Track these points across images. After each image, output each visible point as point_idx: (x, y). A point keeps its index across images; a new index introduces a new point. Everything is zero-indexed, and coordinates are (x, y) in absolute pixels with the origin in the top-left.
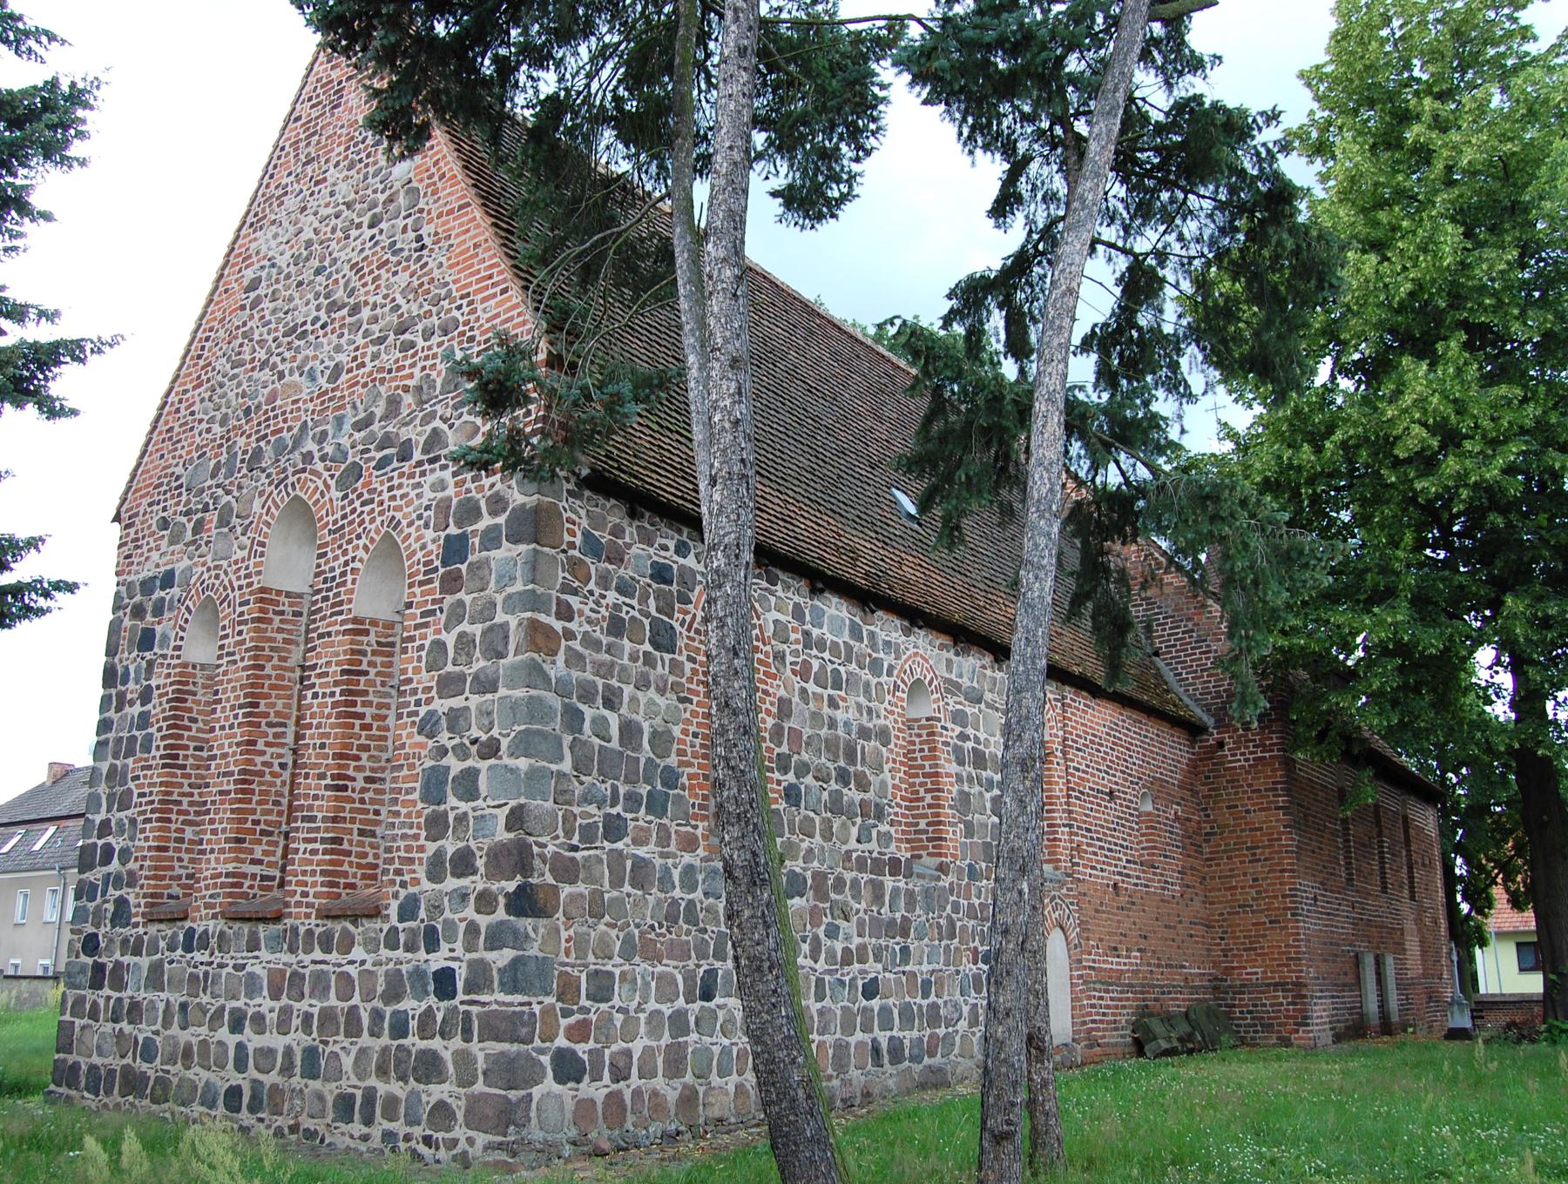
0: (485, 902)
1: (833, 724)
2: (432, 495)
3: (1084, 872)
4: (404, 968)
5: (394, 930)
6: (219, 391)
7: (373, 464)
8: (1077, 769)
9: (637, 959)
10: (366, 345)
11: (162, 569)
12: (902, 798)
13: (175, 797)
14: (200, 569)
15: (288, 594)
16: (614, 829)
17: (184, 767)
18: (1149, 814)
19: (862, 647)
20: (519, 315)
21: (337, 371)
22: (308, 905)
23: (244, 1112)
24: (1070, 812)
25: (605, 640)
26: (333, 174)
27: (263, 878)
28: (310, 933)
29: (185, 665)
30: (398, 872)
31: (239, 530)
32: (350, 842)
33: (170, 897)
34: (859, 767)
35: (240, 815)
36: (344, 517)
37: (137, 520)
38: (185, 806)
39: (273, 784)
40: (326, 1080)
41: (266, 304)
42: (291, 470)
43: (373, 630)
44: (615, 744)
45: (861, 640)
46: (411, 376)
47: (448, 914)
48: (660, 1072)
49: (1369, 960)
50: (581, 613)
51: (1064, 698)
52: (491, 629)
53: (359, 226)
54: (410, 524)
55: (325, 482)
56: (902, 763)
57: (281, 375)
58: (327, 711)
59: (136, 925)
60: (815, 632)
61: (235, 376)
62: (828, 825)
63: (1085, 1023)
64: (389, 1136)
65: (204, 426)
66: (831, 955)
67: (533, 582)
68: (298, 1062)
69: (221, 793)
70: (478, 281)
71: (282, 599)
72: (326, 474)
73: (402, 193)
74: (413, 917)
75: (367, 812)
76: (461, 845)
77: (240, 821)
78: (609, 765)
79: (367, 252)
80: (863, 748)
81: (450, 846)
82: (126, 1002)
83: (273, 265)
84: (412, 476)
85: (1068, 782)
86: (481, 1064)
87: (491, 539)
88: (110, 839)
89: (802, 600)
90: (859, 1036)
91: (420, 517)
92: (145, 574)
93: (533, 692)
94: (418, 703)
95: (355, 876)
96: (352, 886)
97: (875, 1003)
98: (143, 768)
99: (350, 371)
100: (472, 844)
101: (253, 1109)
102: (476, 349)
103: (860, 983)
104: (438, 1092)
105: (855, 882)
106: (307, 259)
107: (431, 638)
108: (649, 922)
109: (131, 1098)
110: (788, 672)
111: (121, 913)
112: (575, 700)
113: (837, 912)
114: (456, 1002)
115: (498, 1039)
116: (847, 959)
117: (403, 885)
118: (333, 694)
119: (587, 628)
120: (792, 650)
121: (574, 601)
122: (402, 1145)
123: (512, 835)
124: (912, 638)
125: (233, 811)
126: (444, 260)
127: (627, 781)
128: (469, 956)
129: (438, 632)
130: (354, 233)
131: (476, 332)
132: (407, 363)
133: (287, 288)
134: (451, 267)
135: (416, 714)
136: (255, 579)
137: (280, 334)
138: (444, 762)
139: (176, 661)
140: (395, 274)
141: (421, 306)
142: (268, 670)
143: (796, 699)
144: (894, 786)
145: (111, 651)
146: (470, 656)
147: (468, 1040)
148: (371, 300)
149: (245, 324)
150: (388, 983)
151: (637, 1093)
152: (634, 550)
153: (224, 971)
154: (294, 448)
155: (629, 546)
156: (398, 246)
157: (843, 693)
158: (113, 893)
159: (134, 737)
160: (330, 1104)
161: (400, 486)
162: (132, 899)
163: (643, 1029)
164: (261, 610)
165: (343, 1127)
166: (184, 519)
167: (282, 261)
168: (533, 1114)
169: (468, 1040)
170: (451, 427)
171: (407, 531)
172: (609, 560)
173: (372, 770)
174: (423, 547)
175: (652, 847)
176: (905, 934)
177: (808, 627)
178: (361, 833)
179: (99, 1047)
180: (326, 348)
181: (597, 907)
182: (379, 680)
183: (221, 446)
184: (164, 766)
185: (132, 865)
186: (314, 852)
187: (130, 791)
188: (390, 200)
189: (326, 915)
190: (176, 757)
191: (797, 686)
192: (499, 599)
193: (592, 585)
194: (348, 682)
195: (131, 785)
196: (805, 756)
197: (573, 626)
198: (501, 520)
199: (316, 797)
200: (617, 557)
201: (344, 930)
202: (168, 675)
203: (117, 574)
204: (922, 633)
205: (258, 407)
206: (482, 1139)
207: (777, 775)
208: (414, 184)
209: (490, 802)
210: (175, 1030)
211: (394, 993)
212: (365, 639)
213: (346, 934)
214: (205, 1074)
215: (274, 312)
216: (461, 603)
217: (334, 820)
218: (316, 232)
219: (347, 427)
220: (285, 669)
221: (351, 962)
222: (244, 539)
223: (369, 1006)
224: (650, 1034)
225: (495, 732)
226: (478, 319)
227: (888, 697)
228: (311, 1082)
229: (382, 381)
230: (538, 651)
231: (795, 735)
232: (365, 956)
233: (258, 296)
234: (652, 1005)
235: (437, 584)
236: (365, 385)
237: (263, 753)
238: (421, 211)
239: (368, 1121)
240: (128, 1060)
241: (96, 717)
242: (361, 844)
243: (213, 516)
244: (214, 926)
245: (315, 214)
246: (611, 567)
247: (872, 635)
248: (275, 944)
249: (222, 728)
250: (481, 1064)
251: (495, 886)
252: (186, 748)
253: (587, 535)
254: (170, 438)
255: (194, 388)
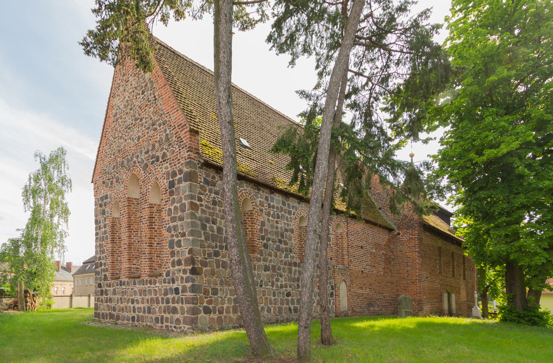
0: (185, 272)
1: (277, 228)
2: (165, 170)
3: (352, 267)
4: (168, 288)
5: (165, 279)
6: (112, 146)
7: (150, 163)
8: (351, 240)
9: (224, 285)
10: (145, 130)
11: (105, 194)
12: (297, 247)
13: (115, 250)
14: (113, 194)
15: (135, 199)
16: (217, 254)
17: (116, 243)
18: (374, 253)
19: (286, 207)
20: (182, 117)
21: (139, 138)
22: (146, 274)
23: (136, 322)
24: (348, 252)
25: (211, 207)
26: (131, 79)
27: (136, 268)
28: (147, 280)
29: (113, 218)
30: (165, 265)
31: (121, 183)
32: (154, 259)
33: (116, 273)
34: (285, 239)
35: (129, 254)
36: (145, 178)
37: (97, 182)
38: (117, 252)
39: (136, 246)
40: (153, 314)
41: (119, 120)
42: (131, 166)
43: (155, 207)
44: (216, 233)
45: (285, 205)
46: (157, 138)
47: (176, 275)
48: (231, 312)
49: (446, 295)
50: (204, 200)
51: (348, 221)
52: (181, 205)
53: (139, 94)
54: (161, 179)
55: (140, 169)
56: (297, 238)
57: (126, 140)
58: (146, 227)
59: (109, 280)
60: (272, 204)
61: (115, 141)
62: (276, 254)
63: (351, 306)
64: (167, 326)
65: (109, 156)
66: (277, 286)
67: (190, 192)
68: (146, 310)
69: (124, 248)
70: (171, 108)
71: (134, 200)
72: (139, 167)
73: (149, 83)
74: (169, 276)
75: (158, 251)
76: (178, 258)
77: (129, 255)
78: (214, 238)
79: (142, 102)
80: (286, 234)
81: (176, 259)
82: (109, 298)
83: (120, 108)
84: (160, 166)
85: (348, 243)
86: (186, 310)
87: (180, 181)
88: (101, 261)
89: (268, 195)
90: (285, 306)
91: (163, 176)
92: (101, 196)
93: (193, 220)
94: (166, 224)
95: (156, 267)
96: (156, 269)
97: (290, 298)
98: (107, 244)
99: (142, 138)
100: (181, 258)
101: (138, 321)
102: (172, 129)
103: (285, 293)
104: (177, 316)
105: (284, 268)
106: (128, 106)
107: (168, 208)
108: (227, 276)
109: (111, 320)
110: (264, 214)
111: (106, 278)
112: (204, 222)
113: (279, 275)
114: (179, 295)
115: (189, 304)
116: (282, 286)
117: (166, 268)
118: (147, 223)
119: (206, 203)
120: (265, 208)
121: (202, 197)
122: (170, 329)
123: (189, 255)
124: (301, 205)
125: (127, 253)
126: (161, 102)
127: (219, 242)
128: (182, 284)
129: (169, 206)
130: (138, 97)
131: (171, 124)
132: (156, 134)
133: (124, 115)
134: (163, 104)
135: (166, 227)
136: (126, 195)
137: (124, 129)
138: (174, 238)
139: (111, 217)
140: (150, 108)
141: (157, 117)
142: (132, 218)
143: (266, 221)
144: (295, 244)
145: (96, 216)
146: (177, 212)
147: (182, 304)
148: (145, 117)
149: (115, 126)
150: (164, 291)
151: (225, 317)
152: (219, 183)
153: (129, 290)
154: (131, 160)
155: (217, 181)
156: (150, 99)
157: (280, 220)
158: (103, 273)
159: (104, 236)
160: (154, 319)
161: (157, 168)
162: (107, 274)
163: (226, 302)
164: (128, 203)
165: (157, 325)
166: (108, 181)
167: (122, 107)
168: (199, 321)
169: (182, 304)
170: (168, 151)
171: (160, 180)
172: (211, 185)
173: (158, 241)
174: (164, 184)
175: (227, 258)
176: (298, 281)
177: (269, 202)
178: (157, 256)
179: (104, 309)
180: (136, 132)
181: (213, 273)
182: (158, 219)
183: (114, 161)
184: (111, 243)
185: (107, 267)
186: (146, 261)
187: (104, 249)
188: (146, 85)
189: (149, 276)
190: (114, 241)
191: (266, 218)
192: (183, 196)
193: (207, 192)
194: (150, 220)
195: (104, 248)
196: (269, 236)
197: (202, 203)
198: (182, 176)
199: (145, 248)
200: (214, 185)
201: (154, 279)
202: (110, 221)
203: (95, 196)
204: (304, 203)
205: (121, 150)
206: (187, 327)
207: (261, 241)
208: (152, 80)
209: (184, 248)
210: (120, 304)
211: (166, 294)
212: (153, 209)
213: (155, 280)
214: (127, 314)
215: (122, 122)
216: (174, 198)
217: (150, 254)
218: (129, 97)
219: (143, 154)
220: (136, 218)
221: (156, 287)
222: (123, 185)
223: (161, 297)
224: (228, 303)
225: (184, 231)
226: (172, 120)
227: (293, 221)
228: (149, 315)
229: (150, 140)
230: (193, 210)
231: (266, 231)
232: (159, 285)
233: (117, 118)
234: (229, 296)
235: (168, 194)
236: (146, 141)
237: (133, 239)
238: (154, 88)
239: (162, 323)
240: (110, 311)
241: (95, 232)
242: (157, 259)
243: (115, 180)
244: (126, 280)
245: (128, 92)
246: (212, 187)
247: (289, 204)
248: (140, 283)
249: (123, 233)
250: (186, 310)
251: (187, 268)
252: (116, 238)
253: (205, 179)
254: (102, 160)
255: (106, 145)
